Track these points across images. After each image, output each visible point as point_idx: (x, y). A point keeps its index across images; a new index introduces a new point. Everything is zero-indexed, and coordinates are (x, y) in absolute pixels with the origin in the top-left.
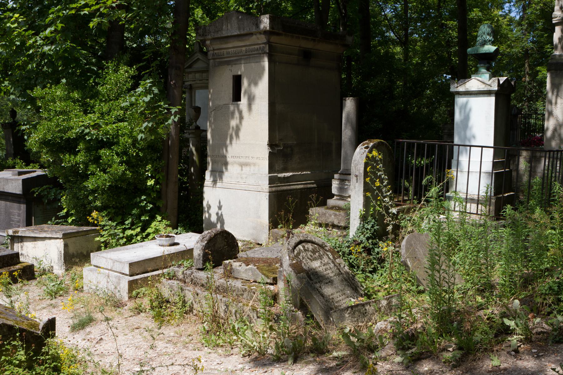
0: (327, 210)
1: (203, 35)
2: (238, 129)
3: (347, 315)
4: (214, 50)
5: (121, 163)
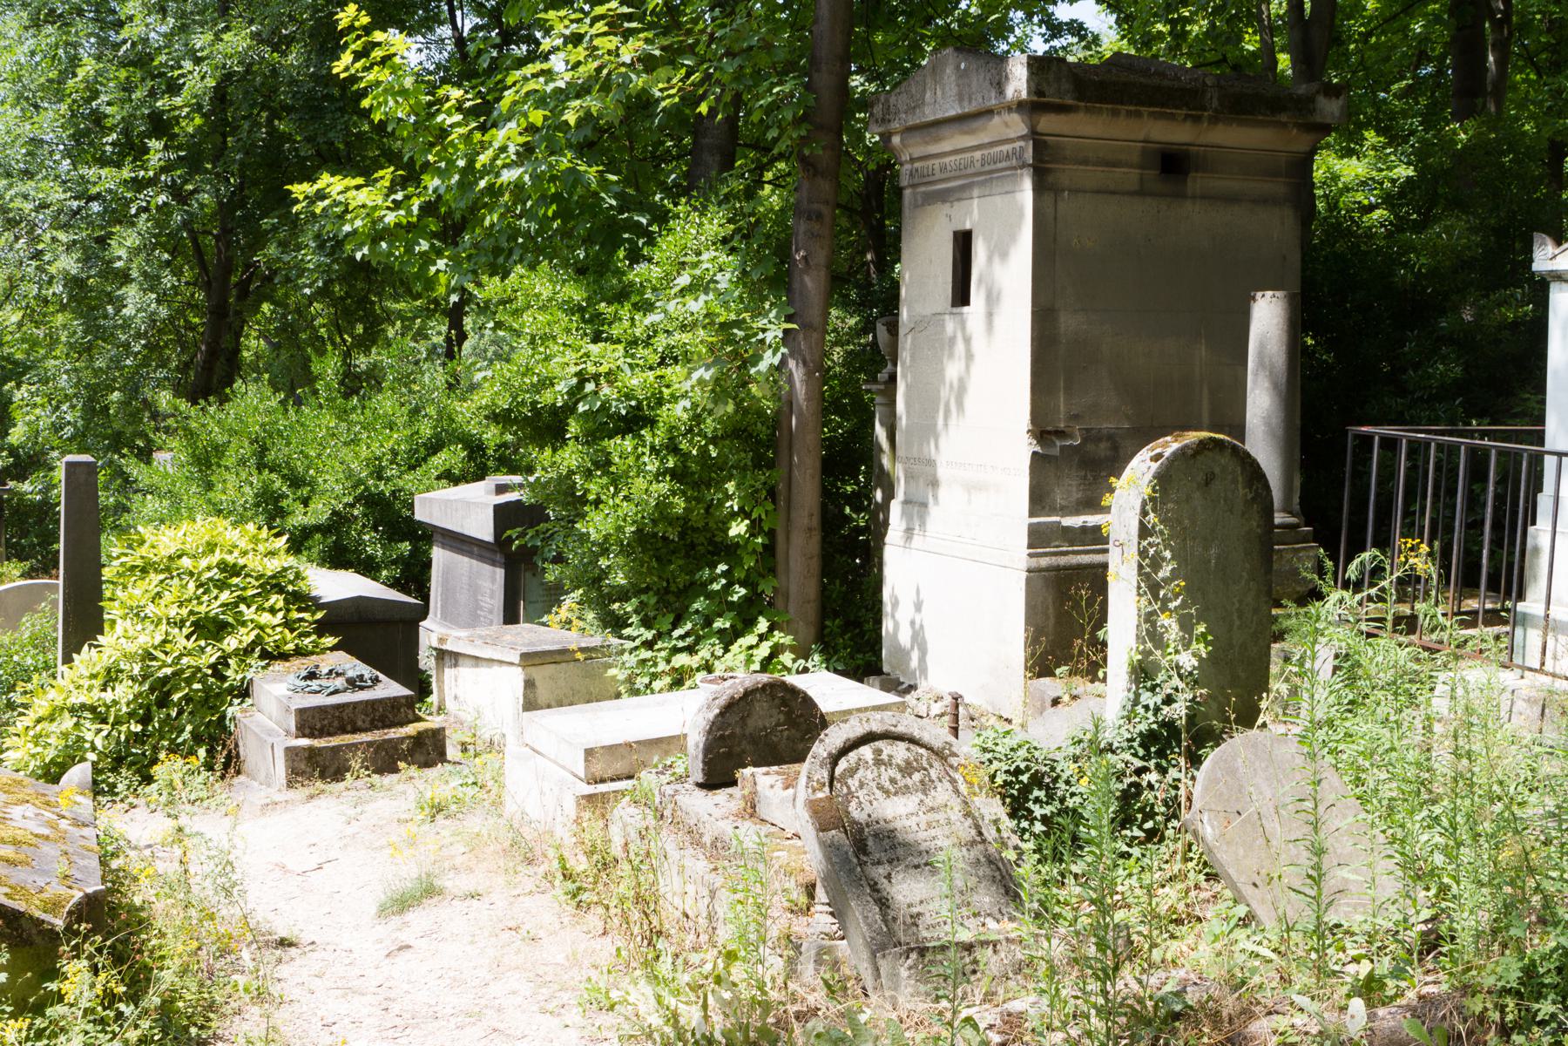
1: (883, 120)
2: (961, 390)
3: (904, 973)
4: (912, 160)
5: (658, 476)
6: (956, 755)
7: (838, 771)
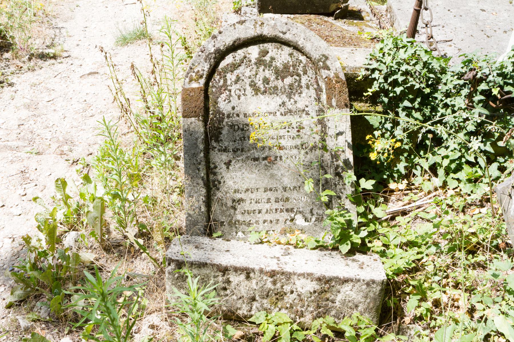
6: (328, 68)
7: (223, 64)
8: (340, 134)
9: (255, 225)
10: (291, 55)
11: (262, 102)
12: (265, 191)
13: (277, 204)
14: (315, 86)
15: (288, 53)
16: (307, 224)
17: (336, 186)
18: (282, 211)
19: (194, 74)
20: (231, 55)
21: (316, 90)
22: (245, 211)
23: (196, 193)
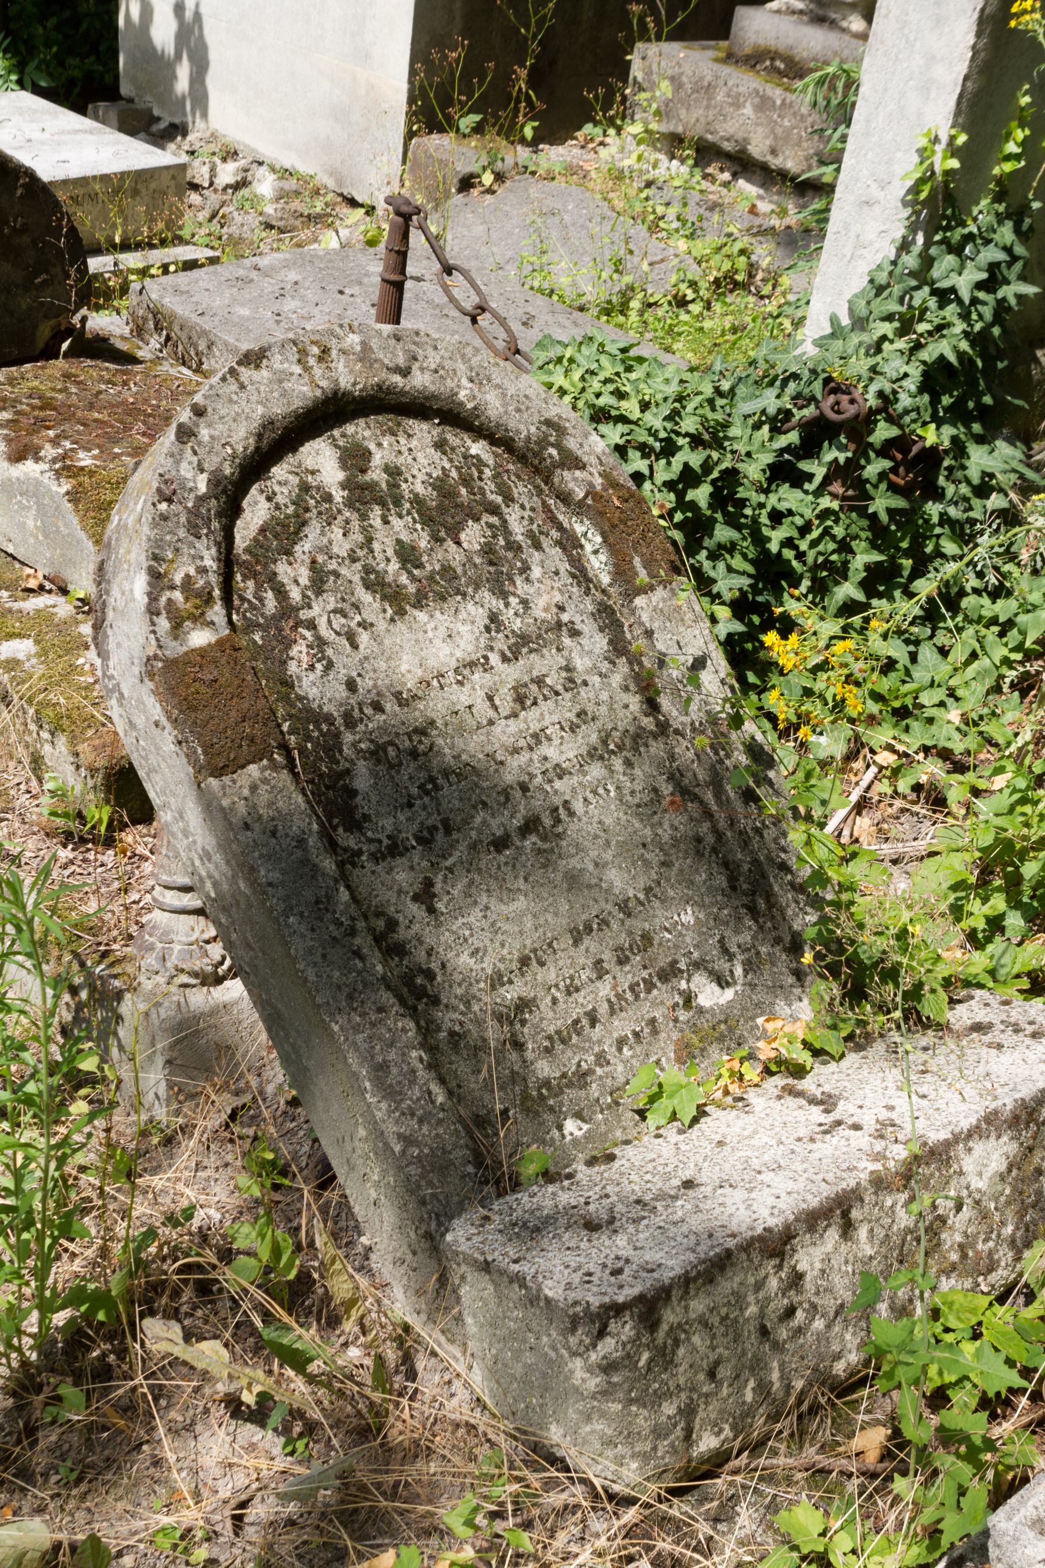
0: (726, 70)
8: (699, 663)
9: (599, 1071)
10: (440, 445)
11: (430, 634)
12: (576, 942)
13: (627, 968)
14: (555, 534)
15: (428, 440)
16: (729, 994)
17: (761, 836)
18: (650, 986)
19: (178, 596)
20: (254, 490)
21: (564, 549)
22: (550, 1038)
23: (391, 1045)
